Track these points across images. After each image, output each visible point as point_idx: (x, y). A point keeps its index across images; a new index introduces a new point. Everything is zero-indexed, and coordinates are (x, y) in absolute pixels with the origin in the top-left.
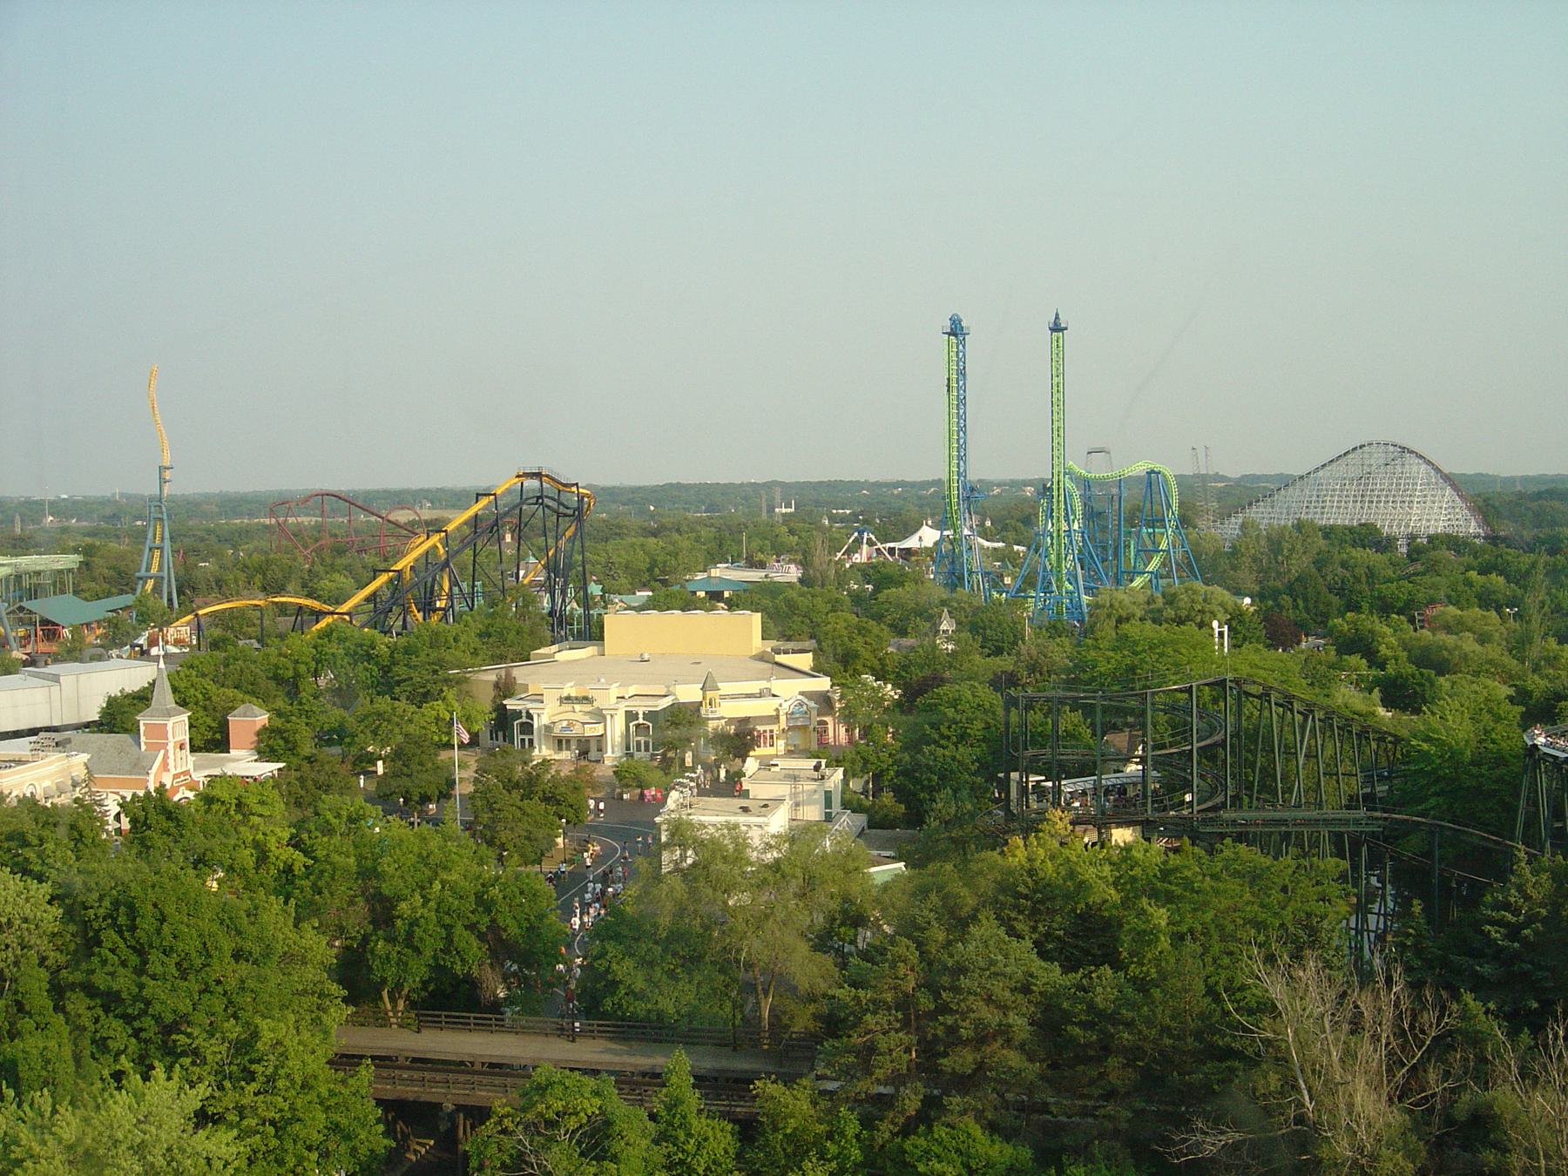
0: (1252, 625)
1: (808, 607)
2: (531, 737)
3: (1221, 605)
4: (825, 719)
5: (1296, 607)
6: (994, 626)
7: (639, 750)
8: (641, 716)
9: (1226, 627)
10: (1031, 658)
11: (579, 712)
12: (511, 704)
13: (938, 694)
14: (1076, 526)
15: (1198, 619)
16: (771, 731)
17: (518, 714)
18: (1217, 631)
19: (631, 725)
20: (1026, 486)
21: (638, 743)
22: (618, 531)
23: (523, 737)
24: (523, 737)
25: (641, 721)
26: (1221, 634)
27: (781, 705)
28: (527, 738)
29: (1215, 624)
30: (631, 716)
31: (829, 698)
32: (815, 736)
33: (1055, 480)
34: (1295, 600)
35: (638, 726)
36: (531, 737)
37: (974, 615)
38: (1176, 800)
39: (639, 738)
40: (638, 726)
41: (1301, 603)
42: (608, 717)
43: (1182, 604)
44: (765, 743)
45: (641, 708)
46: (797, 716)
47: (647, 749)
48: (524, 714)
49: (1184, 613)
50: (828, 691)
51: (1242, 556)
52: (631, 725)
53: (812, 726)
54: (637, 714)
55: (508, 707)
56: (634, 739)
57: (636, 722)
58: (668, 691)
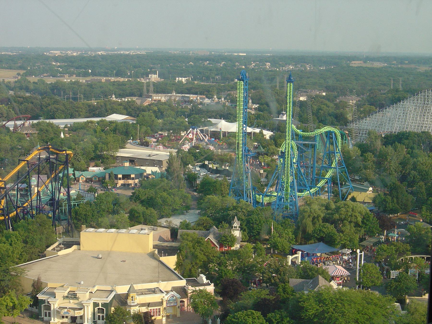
0: (373, 222)
1: (172, 201)
2: (49, 311)
3: (360, 213)
4: (183, 300)
5: (393, 202)
6: (257, 223)
7: (99, 319)
8: (100, 305)
9: (363, 252)
10: (276, 267)
11: (72, 303)
12: (40, 297)
13: (237, 316)
14: (294, 161)
15: (349, 220)
16: (159, 309)
17: (43, 301)
18: (359, 254)
19: (96, 308)
20: (267, 62)
21: (99, 316)
22: (77, 110)
23: (46, 311)
24: (46, 311)
25: (100, 307)
26: (361, 256)
27: (164, 297)
28: (48, 312)
29: (358, 251)
30: (96, 305)
31: (185, 290)
32: (179, 310)
33: (287, 150)
34: (392, 199)
35: (99, 309)
36: (49, 311)
37: (249, 215)
38: (338, 82)
39: (99, 314)
40: (99, 309)
41: (395, 200)
42: (86, 307)
43: (342, 212)
44: (156, 314)
45: (100, 302)
46: (171, 301)
47: (103, 319)
48: (46, 302)
49: (343, 217)
50: (185, 286)
51: (369, 161)
52: (96, 308)
53: (178, 306)
54: (99, 304)
55: (39, 298)
56: (97, 315)
57: (98, 307)
58: (112, 288)
